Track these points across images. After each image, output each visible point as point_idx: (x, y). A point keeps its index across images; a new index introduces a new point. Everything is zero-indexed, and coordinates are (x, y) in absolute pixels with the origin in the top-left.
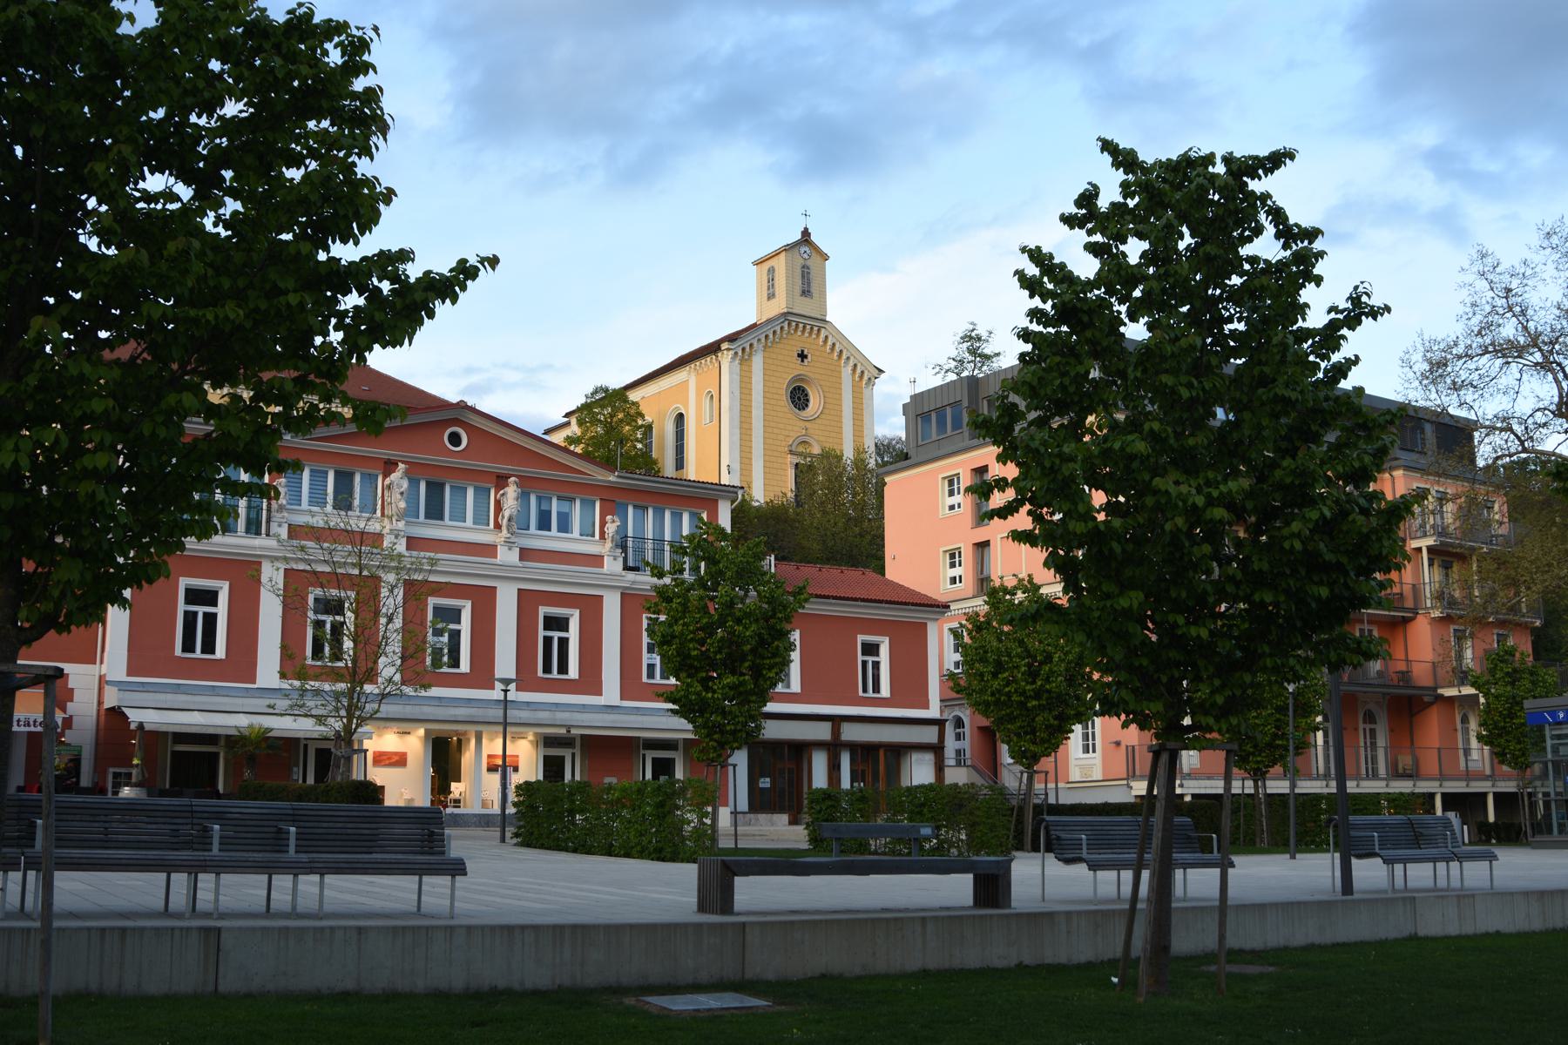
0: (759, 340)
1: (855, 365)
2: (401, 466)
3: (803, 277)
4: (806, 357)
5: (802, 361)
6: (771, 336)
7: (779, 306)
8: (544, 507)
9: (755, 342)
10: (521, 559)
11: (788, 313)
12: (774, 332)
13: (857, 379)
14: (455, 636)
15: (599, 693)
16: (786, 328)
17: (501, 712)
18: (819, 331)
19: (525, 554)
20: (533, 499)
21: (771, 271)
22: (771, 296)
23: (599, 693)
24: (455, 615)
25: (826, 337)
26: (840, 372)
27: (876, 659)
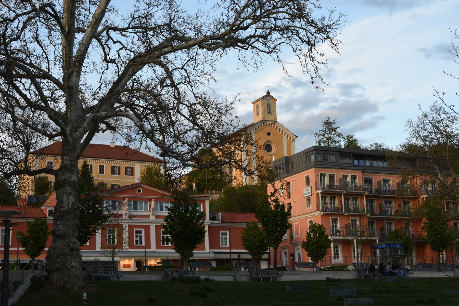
0: (253, 130)
1: (288, 136)
2: (127, 199)
3: (268, 107)
4: (270, 134)
5: (269, 136)
6: (257, 129)
7: (260, 118)
8: (162, 205)
9: (252, 131)
10: (156, 218)
11: (263, 120)
12: (259, 127)
13: (289, 140)
14: (141, 237)
15: (150, 248)
16: (263, 125)
17: (144, 254)
18: (274, 125)
19: (157, 217)
20: (159, 203)
21: (257, 106)
22: (258, 114)
23: (150, 248)
24: (140, 232)
25: (277, 127)
26: (282, 138)
27: (226, 237)
